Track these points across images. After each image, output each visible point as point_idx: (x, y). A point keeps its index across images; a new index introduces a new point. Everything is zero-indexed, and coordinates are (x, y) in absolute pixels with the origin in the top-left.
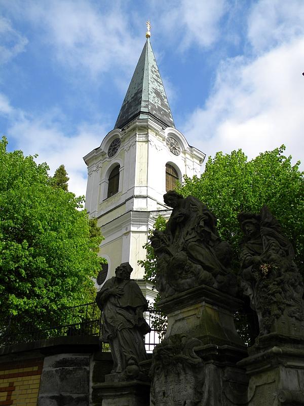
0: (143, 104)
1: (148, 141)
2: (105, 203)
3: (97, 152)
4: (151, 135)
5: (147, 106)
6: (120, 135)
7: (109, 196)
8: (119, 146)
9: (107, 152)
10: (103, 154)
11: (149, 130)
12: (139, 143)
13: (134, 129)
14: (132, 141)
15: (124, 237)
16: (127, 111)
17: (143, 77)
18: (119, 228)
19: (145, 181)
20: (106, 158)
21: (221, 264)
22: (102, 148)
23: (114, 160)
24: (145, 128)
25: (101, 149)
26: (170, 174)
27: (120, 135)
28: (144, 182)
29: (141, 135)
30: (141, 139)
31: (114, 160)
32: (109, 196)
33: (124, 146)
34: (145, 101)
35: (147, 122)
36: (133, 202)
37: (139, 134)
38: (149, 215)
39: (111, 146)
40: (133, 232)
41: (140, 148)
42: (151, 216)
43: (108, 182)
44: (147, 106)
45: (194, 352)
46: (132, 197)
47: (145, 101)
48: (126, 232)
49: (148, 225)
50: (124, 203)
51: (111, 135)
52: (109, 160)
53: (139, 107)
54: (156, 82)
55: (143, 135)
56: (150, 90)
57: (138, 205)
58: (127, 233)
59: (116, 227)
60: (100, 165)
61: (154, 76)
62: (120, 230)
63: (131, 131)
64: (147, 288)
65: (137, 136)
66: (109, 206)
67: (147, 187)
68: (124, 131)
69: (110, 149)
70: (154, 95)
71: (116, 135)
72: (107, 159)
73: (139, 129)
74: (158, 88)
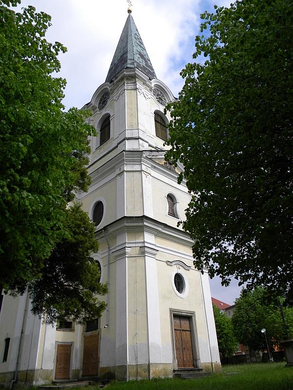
0: (129, 62)
1: (136, 89)
2: (98, 151)
3: (88, 108)
4: (139, 85)
5: (133, 63)
6: (108, 87)
7: (101, 145)
8: (109, 98)
9: (97, 106)
10: (94, 108)
11: (137, 79)
12: (128, 91)
13: (122, 79)
14: (121, 90)
15: (118, 178)
16: (115, 70)
17: (127, 42)
18: (113, 169)
19: (135, 125)
20: (96, 112)
21: (79, 351)
22: (93, 103)
23: (104, 112)
24: (133, 77)
25: (92, 104)
26: (158, 122)
27: (108, 87)
28: (135, 126)
29: (129, 83)
30: (130, 87)
31: (104, 112)
32: (101, 145)
33: (114, 96)
34: (131, 60)
35: (134, 71)
36: (125, 144)
37: (127, 83)
38: (142, 155)
39: (101, 100)
40: (126, 171)
41: (128, 95)
42: (144, 155)
43: (100, 132)
44: (133, 63)
45: (86, 332)
46: (124, 139)
47: (131, 60)
48: (120, 172)
49: (141, 164)
50: (117, 147)
51: (101, 89)
52: (100, 112)
53: (125, 64)
54: (139, 47)
55: (131, 83)
56: (135, 51)
57: (129, 145)
58: (121, 173)
59: (109, 170)
60: (91, 119)
61: (138, 42)
62: (114, 172)
63: (119, 81)
64: (145, 224)
65: (126, 84)
66: (101, 153)
67: (138, 129)
68: (112, 83)
69: (100, 103)
70: (138, 55)
71: (106, 88)
72: (98, 112)
73: (127, 79)
74: (142, 51)
